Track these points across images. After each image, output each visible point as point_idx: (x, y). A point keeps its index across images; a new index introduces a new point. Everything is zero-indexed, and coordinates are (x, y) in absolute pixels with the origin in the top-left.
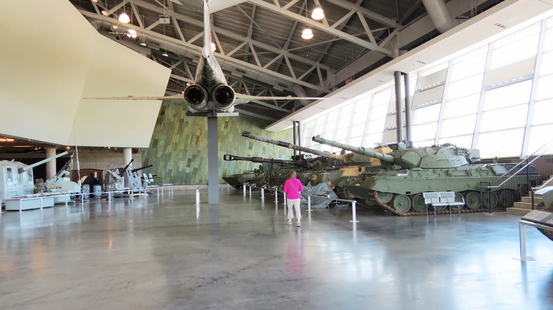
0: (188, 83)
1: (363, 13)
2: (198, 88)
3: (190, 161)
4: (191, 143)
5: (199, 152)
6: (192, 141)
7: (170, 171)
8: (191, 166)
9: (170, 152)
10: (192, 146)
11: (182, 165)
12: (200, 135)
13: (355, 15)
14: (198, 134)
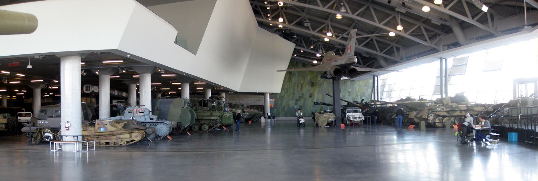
0: (302, 50)
1: (424, 27)
2: (340, 69)
3: (297, 100)
4: (297, 88)
5: (303, 94)
6: (298, 87)
7: (284, 107)
8: (298, 104)
9: (283, 94)
10: (298, 91)
11: (292, 103)
12: (304, 83)
13: (419, 27)
14: (302, 83)
